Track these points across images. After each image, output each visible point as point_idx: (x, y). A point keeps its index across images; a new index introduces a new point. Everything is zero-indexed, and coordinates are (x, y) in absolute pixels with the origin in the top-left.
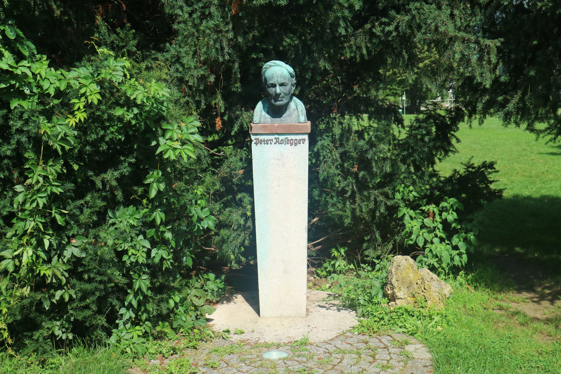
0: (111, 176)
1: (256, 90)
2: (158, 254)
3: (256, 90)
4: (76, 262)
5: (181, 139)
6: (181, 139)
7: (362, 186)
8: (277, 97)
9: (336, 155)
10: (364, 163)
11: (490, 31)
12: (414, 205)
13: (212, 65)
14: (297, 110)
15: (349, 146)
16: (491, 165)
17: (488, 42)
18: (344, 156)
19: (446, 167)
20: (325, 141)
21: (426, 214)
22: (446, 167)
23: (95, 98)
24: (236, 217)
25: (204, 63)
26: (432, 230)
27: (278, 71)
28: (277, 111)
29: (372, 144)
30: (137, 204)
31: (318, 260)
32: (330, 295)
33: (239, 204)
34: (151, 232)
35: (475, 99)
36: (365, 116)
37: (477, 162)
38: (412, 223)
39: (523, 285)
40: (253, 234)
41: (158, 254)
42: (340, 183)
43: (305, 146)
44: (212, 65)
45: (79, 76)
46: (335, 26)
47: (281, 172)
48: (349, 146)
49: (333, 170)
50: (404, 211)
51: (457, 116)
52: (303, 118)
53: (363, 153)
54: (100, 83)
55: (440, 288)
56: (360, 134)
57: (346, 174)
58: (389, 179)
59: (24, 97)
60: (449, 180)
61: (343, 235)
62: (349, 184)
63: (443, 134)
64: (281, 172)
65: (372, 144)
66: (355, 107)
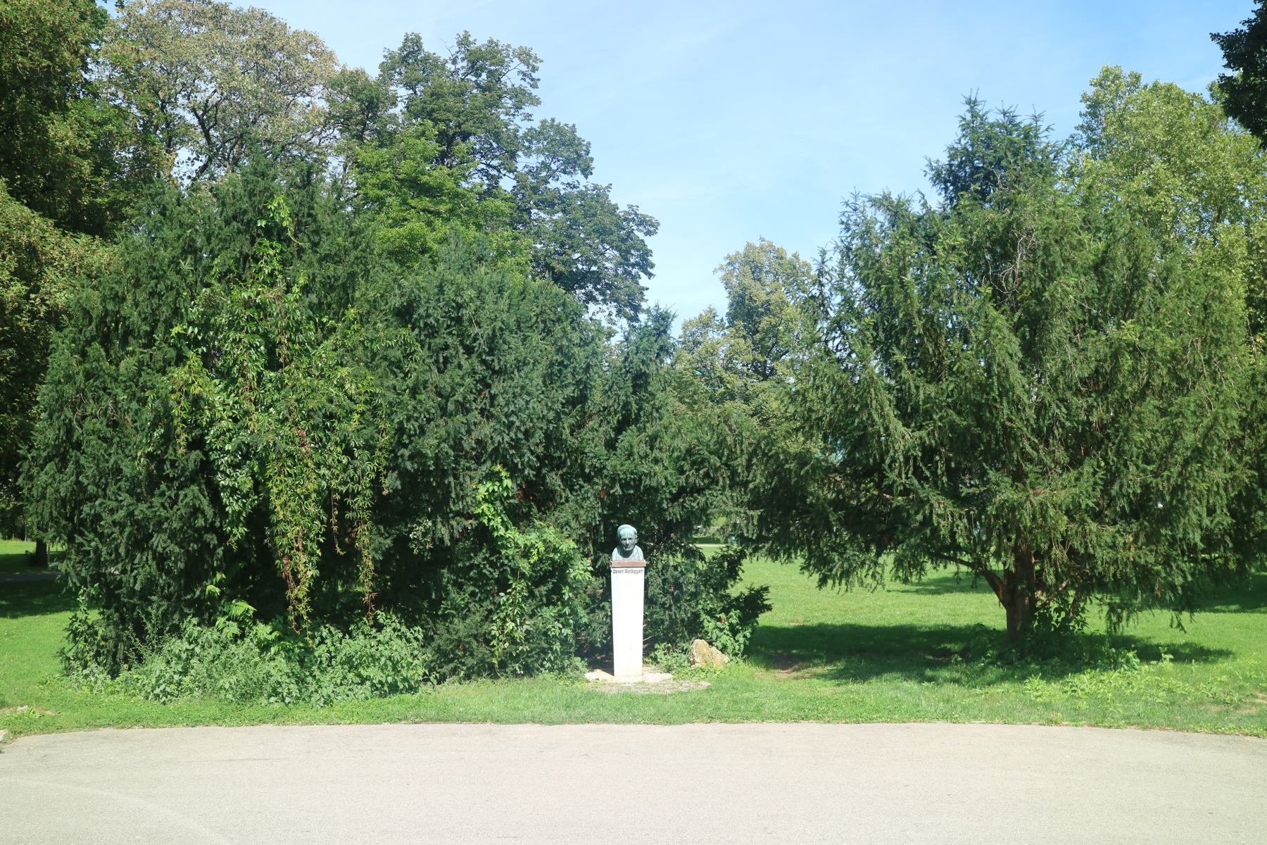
0: (543, 589)
1: (614, 541)
2: (566, 631)
3: (614, 541)
4: (528, 632)
5: (580, 570)
6: (580, 570)
7: (677, 600)
8: (627, 546)
9: (660, 581)
10: (678, 586)
11: (752, 505)
12: (711, 613)
13: (588, 526)
14: (638, 553)
15: (668, 575)
16: (766, 589)
17: (751, 513)
18: (664, 581)
19: (736, 590)
20: (653, 573)
21: (719, 620)
22: (736, 590)
23: (542, 549)
24: (600, 615)
25: (584, 525)
26: (721, 630)
27: (627, 531)
28: (626, 554)
29: (682, 574)
30: (555, 604)
31: (649, 650)
32: (574, 328)
33: (603, 608)
34: (562, 620)
35: (751, 544)
36: (679, 555)
37: (757, 587)
38: (709, 624)
39: (784, 667)
40: (611, 627)
41: (566, 631)
42: (662, 599)
43: (641, 577)
44: (588, 526)
45: (533, 537)
46: (661, 503)
47: (628, 588)
48: (668, 575)
49: (657, 591)
50: (703, 616)
51: (742, 555)
52: (642, 557)
53: (676, 579)
54: (544, 541)
55: (721, 659)
56: (675, 568)
57: (665, 593)
58: (695, 595)
59: (507, 548)
60: (737, 599)
61: (667, 631)
62: (668, 600)
63: (731, 567)
64: (628, 588)
65: (682, 574)
66: (671, 550)
